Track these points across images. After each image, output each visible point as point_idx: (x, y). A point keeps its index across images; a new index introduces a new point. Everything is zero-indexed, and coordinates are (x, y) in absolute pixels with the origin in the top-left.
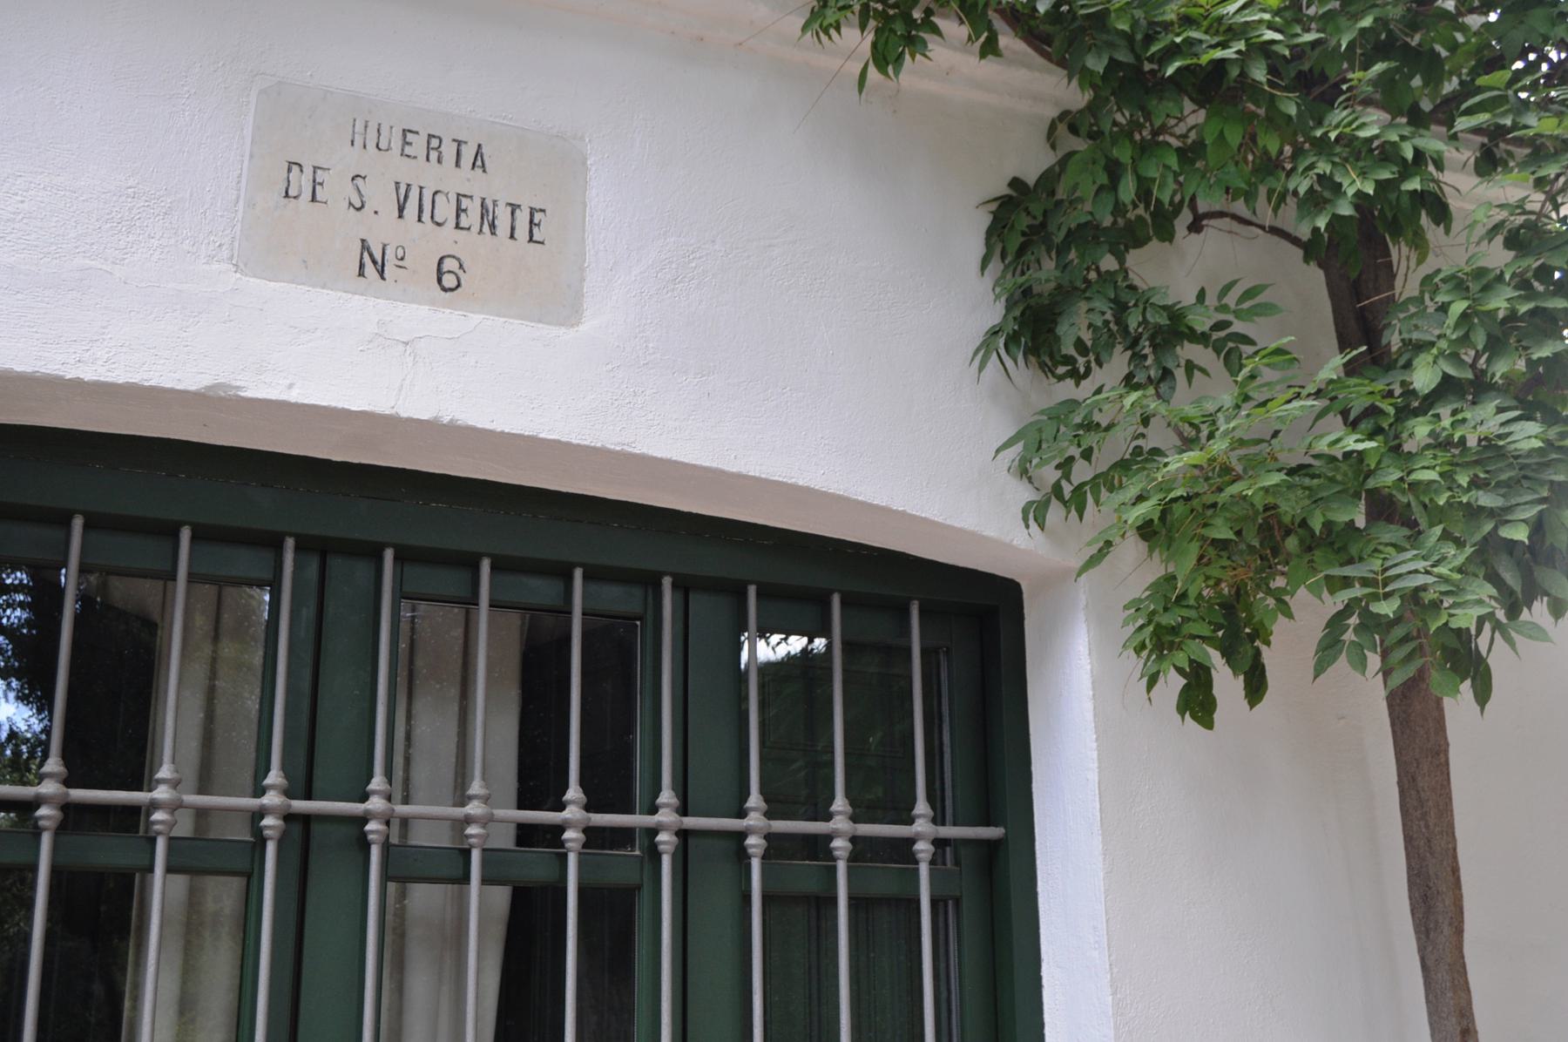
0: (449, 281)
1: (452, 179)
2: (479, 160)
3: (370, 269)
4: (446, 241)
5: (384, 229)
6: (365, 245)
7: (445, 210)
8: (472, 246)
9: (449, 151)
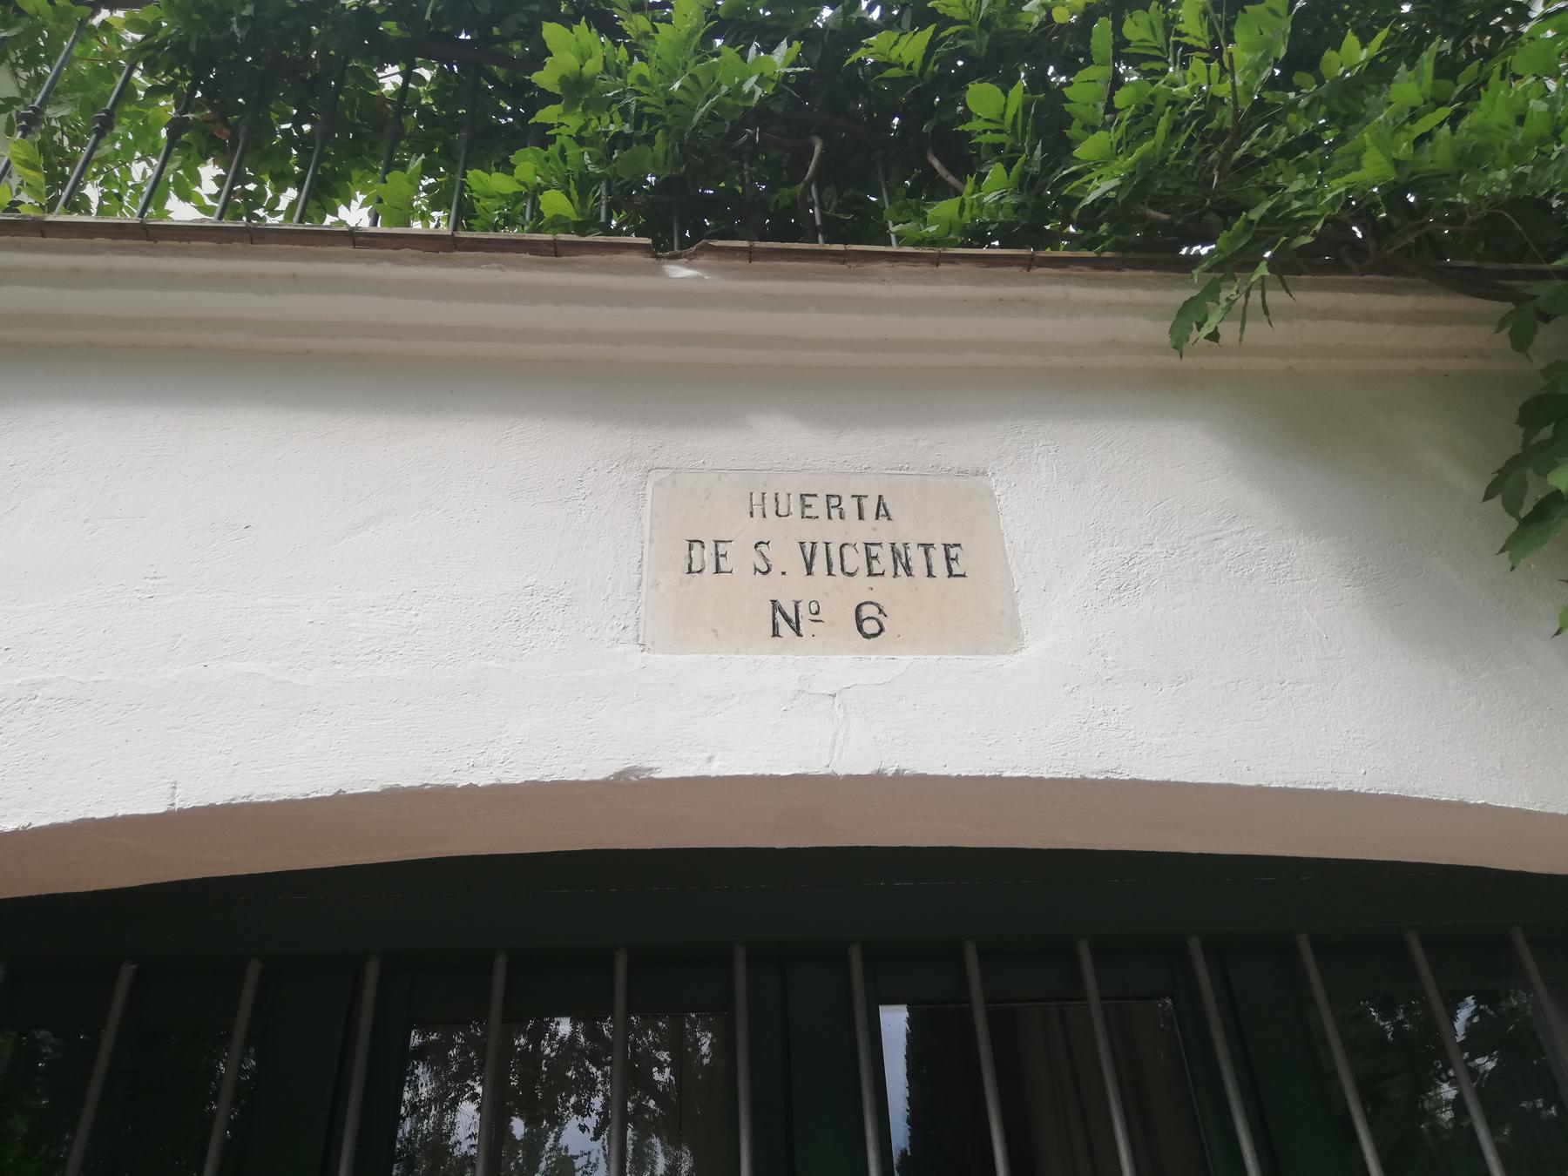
0: (870, 627)
3: (784, 628)
4: (861, 588)
5: (793, 587)
7: (855, 560)
8: (889, 590)
9: (850, 506)
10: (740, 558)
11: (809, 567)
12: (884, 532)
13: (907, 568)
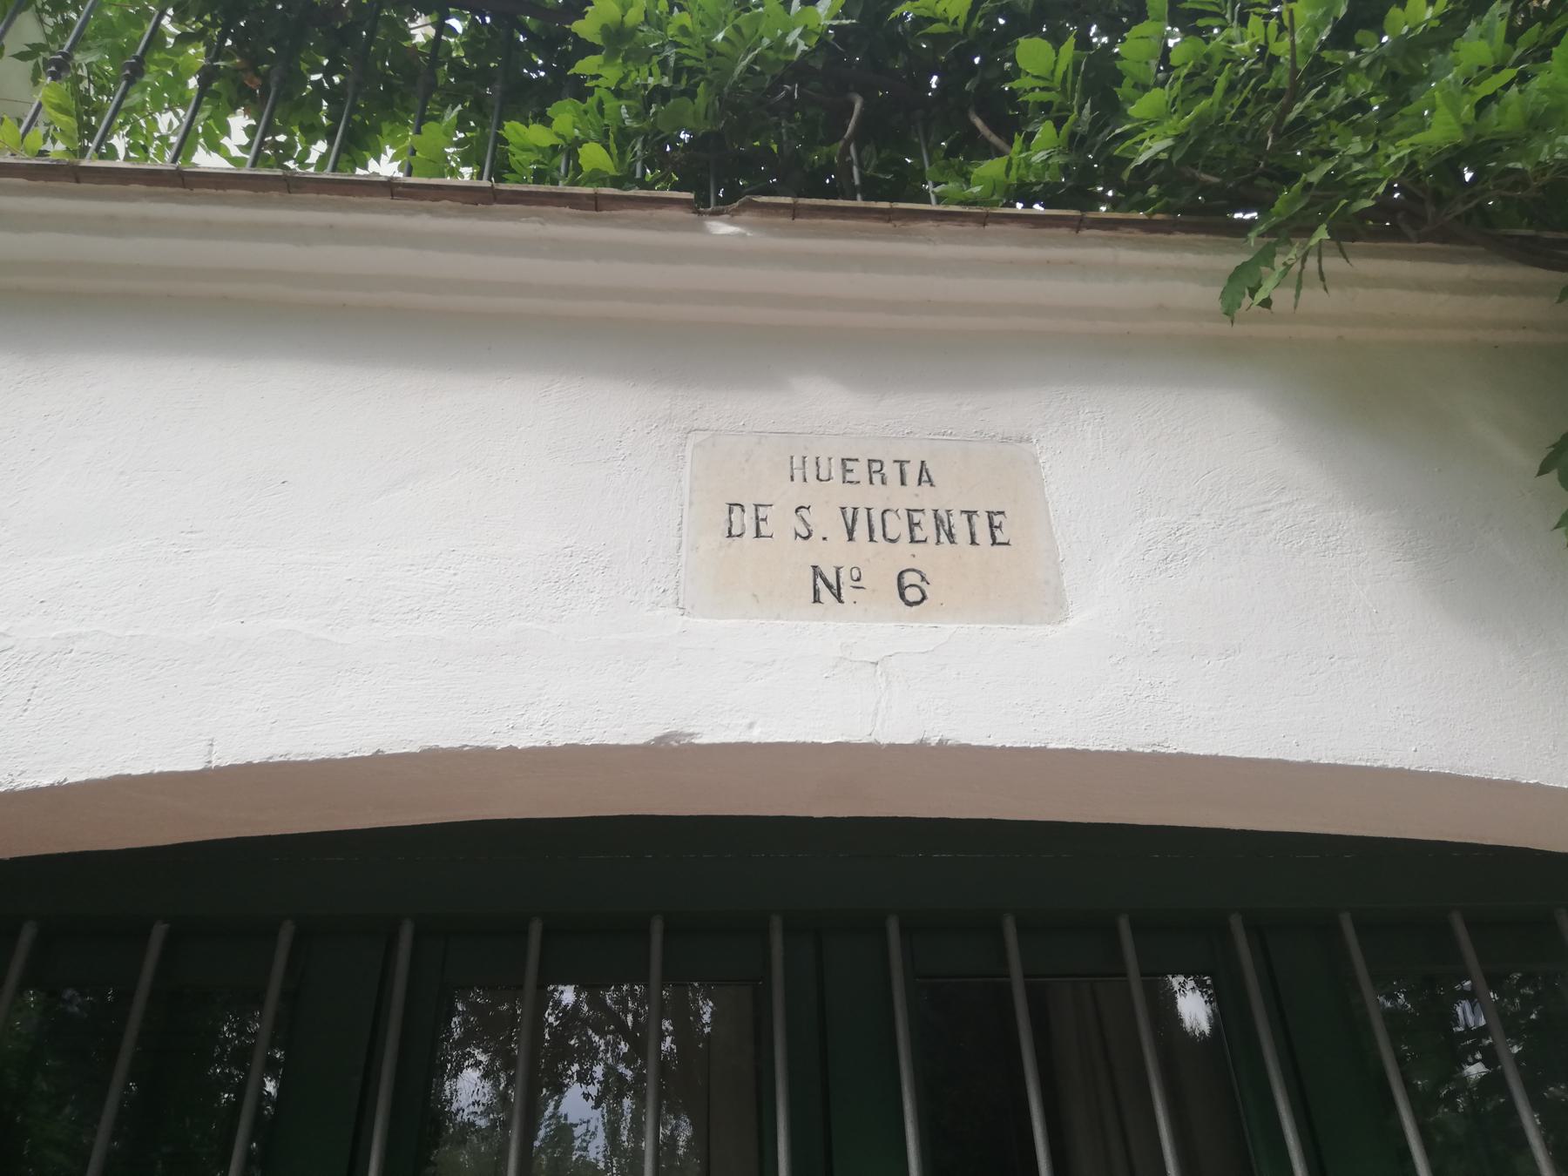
0: (913, 595)
1: (903, 498)
2: (924, 476)
3: (825, 594)
4: (904, 554)
5: (834, 553)
7: (897, 526)
8: (930, 557)
9: (892, 472)
10: (781, 522)
12: (927, 499)
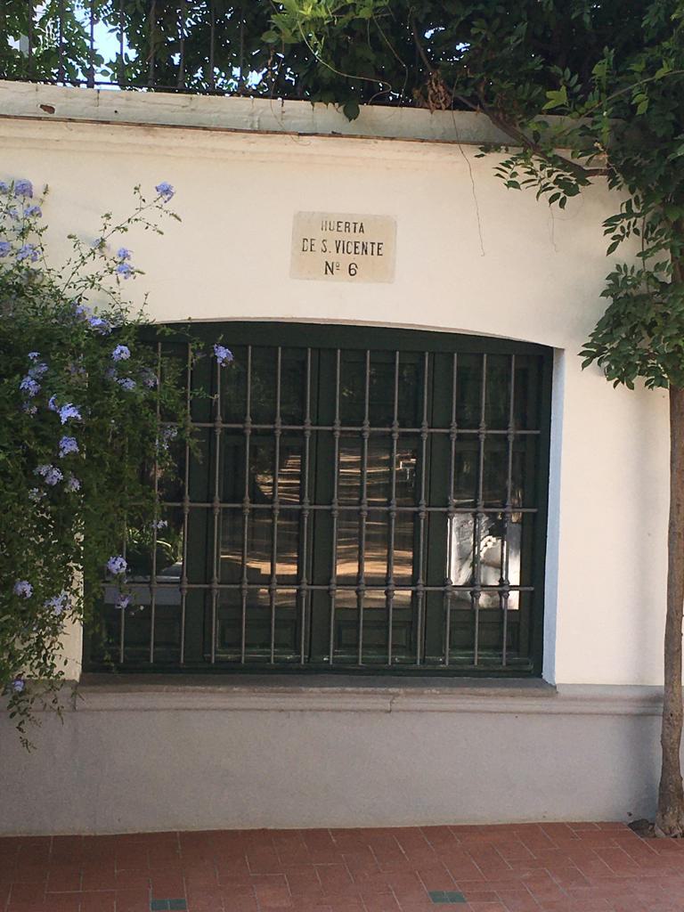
0: (353, 272)
4: (352, 258)
5: (332, 257)
6: (327, 264)
7: (351, 248)
8: (359, 259)
11: (362, 226)
12: (360, 237)
13: (363, 244)
